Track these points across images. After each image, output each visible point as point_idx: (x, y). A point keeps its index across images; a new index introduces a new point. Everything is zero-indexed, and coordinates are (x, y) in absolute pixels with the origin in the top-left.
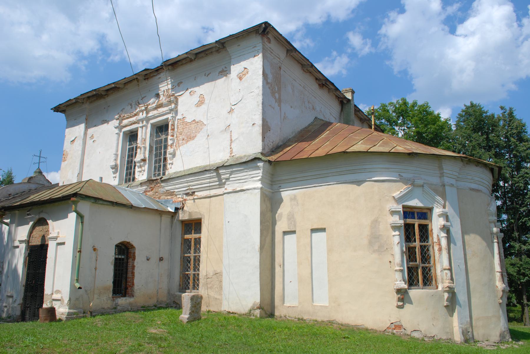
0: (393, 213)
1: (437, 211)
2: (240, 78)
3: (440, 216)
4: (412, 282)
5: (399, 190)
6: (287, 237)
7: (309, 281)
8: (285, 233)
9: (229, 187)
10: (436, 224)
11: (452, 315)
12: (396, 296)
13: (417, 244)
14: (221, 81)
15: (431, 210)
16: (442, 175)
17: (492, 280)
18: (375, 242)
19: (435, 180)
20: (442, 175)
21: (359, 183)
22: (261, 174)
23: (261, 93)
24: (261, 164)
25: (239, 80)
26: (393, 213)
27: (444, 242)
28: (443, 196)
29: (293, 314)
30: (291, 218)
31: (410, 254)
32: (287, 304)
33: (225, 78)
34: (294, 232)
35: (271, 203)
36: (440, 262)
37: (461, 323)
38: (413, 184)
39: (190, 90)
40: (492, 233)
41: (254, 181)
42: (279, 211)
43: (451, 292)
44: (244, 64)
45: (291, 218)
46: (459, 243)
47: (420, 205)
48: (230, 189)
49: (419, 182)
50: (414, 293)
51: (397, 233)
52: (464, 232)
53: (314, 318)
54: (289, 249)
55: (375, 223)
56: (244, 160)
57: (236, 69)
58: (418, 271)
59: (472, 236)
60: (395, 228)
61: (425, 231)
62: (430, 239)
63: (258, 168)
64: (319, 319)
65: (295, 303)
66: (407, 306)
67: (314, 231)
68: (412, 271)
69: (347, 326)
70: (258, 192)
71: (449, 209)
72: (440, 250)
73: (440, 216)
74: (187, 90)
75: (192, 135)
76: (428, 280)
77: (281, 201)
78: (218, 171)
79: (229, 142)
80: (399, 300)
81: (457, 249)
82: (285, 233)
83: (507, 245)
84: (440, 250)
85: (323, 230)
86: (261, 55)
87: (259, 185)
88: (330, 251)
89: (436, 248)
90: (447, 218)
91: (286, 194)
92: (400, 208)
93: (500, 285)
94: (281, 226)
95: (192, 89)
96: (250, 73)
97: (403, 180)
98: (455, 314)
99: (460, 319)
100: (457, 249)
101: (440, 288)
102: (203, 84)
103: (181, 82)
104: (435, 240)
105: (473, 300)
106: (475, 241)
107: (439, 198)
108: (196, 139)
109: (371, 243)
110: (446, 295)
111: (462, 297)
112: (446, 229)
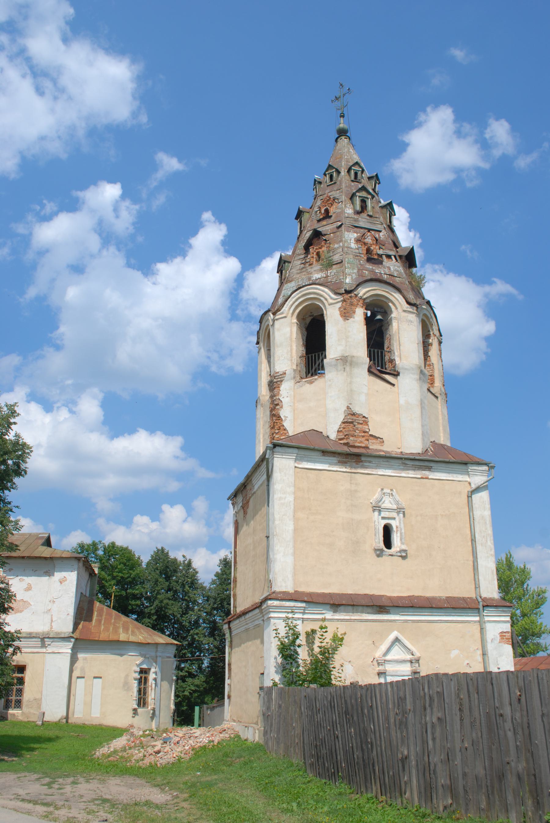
0: (135, 672)
1: (153, 670)
2: (61, 583)
3: (153, 673)
4: (139, 705)
5: (139, 660)
6: (79, 680)
7: (88, 704)
8: (78, 677)
9: (50, 650)
10: (152, 676)
11: (152, 721)
12: (132, 712)
13: (142, 686)
14: (45, 579)
15: (150, 669)
16: (157, 651)
17: (169, 704)
18: (126, 686)
19: (153, 654)
20: (157, 651)
21: (121, 655)
22: (72, 645)
23: (74, 596)
24: (73, 640)
25: (59, 583)
26: (135, 672)
27: (154, 686)
28: (156, 662)
29: (79, 722)
30: (83, 669)
31: (139, 691)
32: (76, 716)
33: (48, 577)
34: (83, 677)
35: (74, 660)
36: (151, 695)
37: (156, 725)
38: (145, 657)
39: (19, 577)
40: (172, 679)
41: (67, 648)
42: (76, 665)
43: (154, 710)
44: (64, 574)
45: (83, 669)
46: (159, 686)
47: (146, 667)
48: (50, 651)
49: (147, 656)
50: (140, 710)
51: (136, 682)
52: (162, 680)
53: (91, 723)
54: (80, 686)
55: (127, 676)
56: (63, 636)
57: (58, 575)
58: (142, 701)
59: (165, 682)
60: (135, 679)
61: (146, 679)
62: (147, 684)
63: (71, 642)
64: (94, 724)
65: (80, 716)
66: (136, 716)
67: (95, 677)
68: (140, 699)
69: (109, 726)
70: (69, 655)
71: (157, 670)
72: (152, 689)
73: (153, 673)
74: (17, 576)
75: (20, 609)
76: (144, 704)
77: (77, 659)
78: (44, 639)
79: (50, 621)
80: (134, 714)
81: (158, 689)
82: (78, 677)
83: (199, 773)
84: (152, 689)
85: (101, 678)
86: (76, 572)
87: (70, 651)
88: (103, 689)
89: (150, 688)
90: (156, 673)
91: (80, 656)
92: (138, 670)
93: (173, 707)
94: (76, 674)
95: (21, 577)
96: (68, 581)
97: (141, 655)
98: (154, 721)
99: (156, 723)
100: (158, 689)
101: (149, 708)
102: (31, 576)
103: (12, 569)
104: (150, 684)
105: (161, 714)
106: (165, 684)
107: (154, 664)
108: (23, 613)
109: (124, 686)
110: (152, 712)
111: (157, 713)
112: (155, 679)
